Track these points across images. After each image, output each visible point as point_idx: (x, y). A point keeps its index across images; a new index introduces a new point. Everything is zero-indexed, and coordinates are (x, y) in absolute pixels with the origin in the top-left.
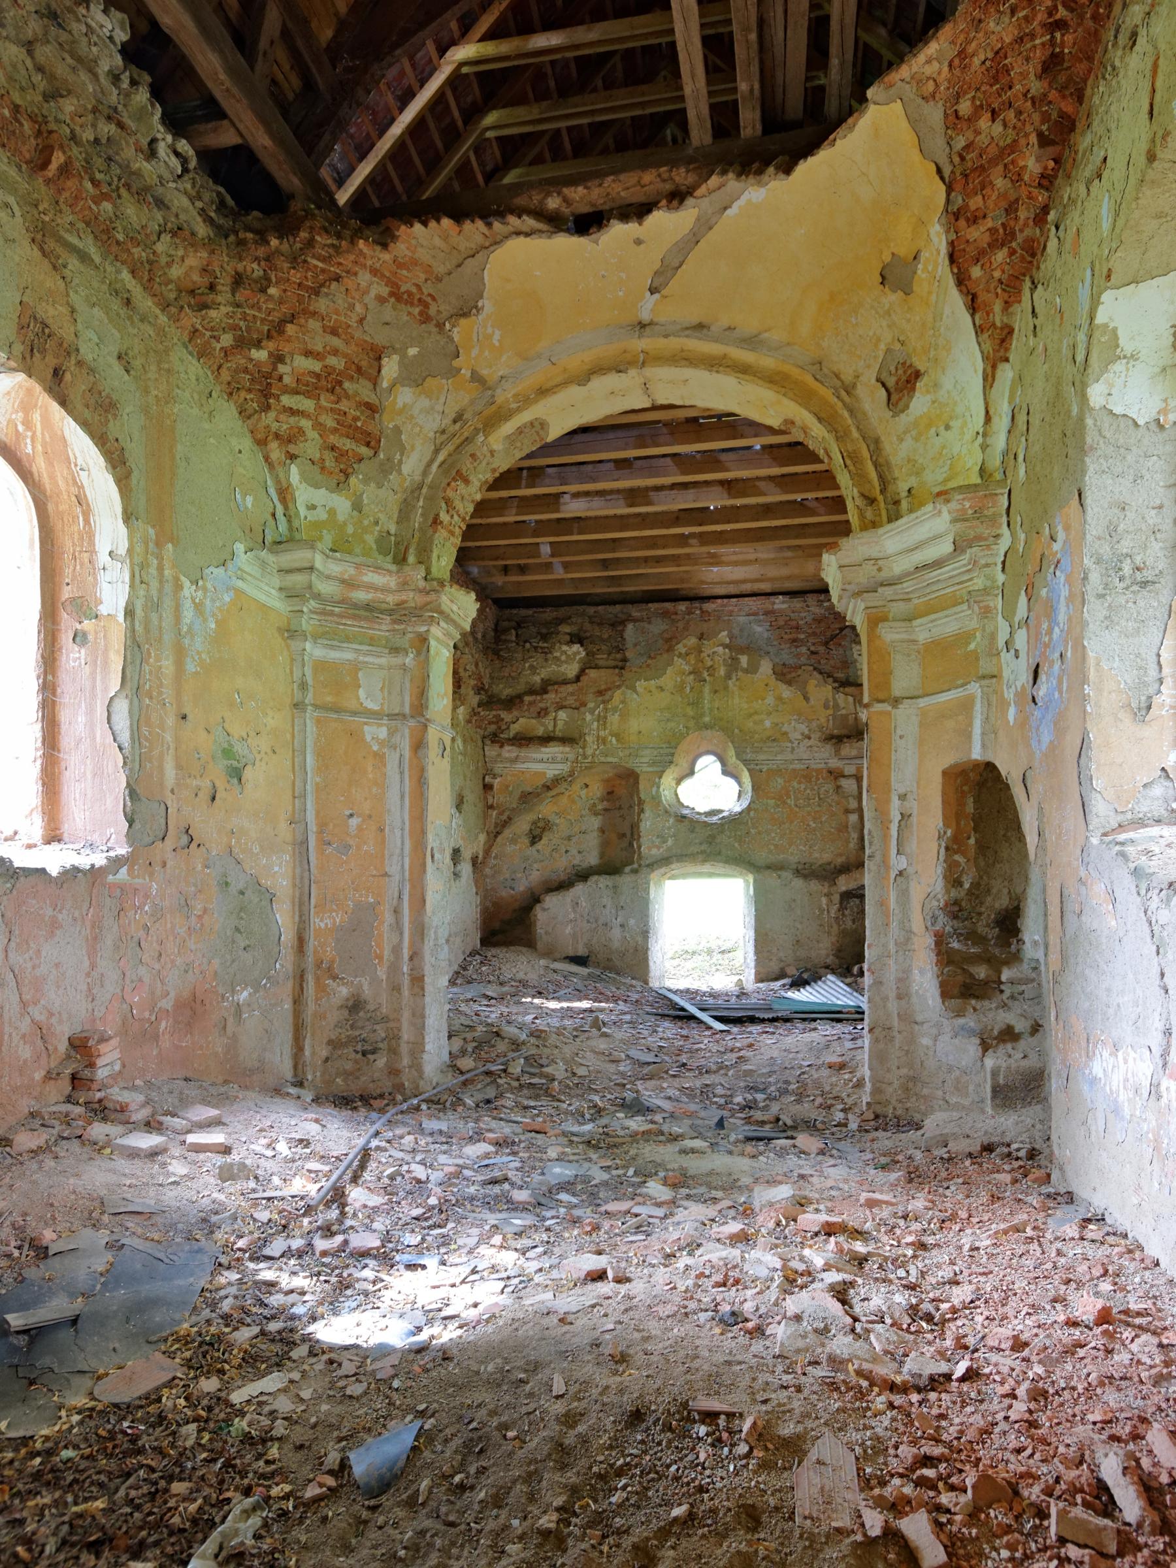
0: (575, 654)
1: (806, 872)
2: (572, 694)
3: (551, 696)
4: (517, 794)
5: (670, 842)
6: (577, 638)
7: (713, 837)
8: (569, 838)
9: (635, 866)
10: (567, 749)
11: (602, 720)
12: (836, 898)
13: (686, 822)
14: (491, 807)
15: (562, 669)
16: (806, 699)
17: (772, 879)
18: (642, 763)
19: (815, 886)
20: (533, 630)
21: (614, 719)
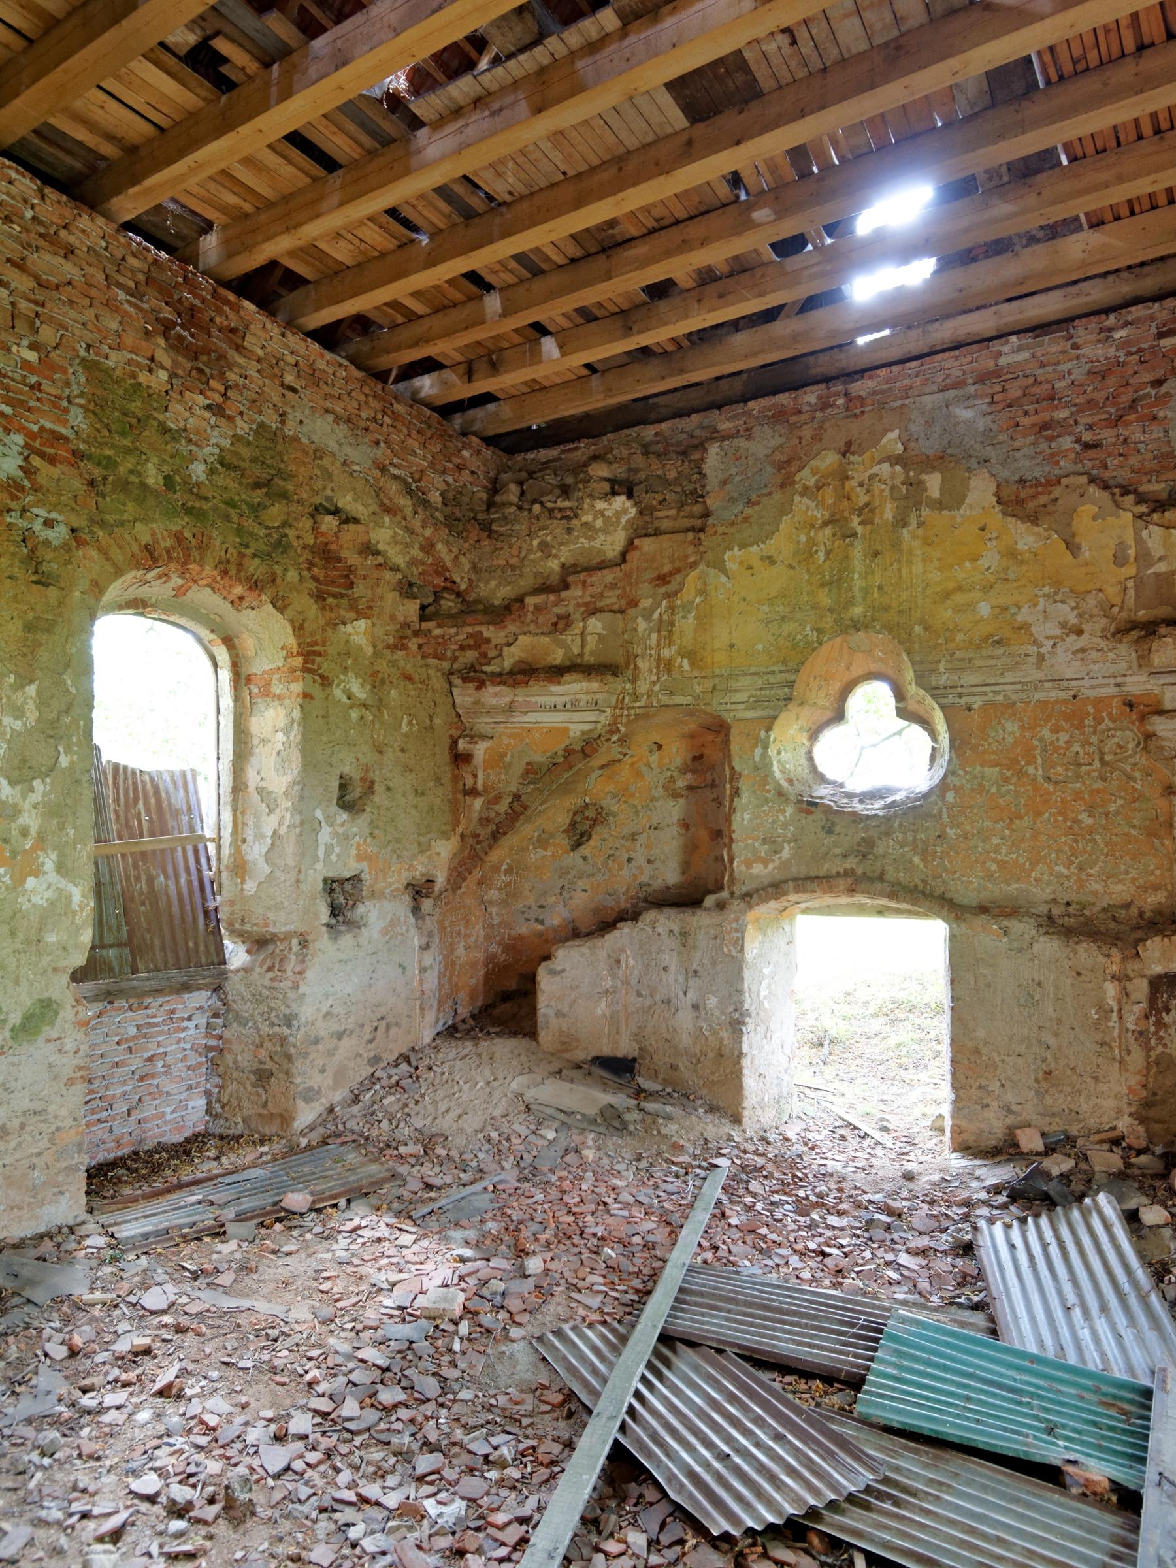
0: (618, 514)
1: (1072, 925)
2: (613, 586)
3: (575, 593)
4: (519, 768)
5: (786, 853)
6: (624, 487)
7: (869, 843)
8: (633, 837)
9: (725, 894)
10: (595, 685)
11: (665, 629)
12: (1141, 988)
13: (818, 815)
14: (473, 792)
15: (597, 543)
16: (1072, 546)
17: (987, 936)
18: (736, 707)
19: (1086, 953)
20: (552, 480)
21: (686, 625)
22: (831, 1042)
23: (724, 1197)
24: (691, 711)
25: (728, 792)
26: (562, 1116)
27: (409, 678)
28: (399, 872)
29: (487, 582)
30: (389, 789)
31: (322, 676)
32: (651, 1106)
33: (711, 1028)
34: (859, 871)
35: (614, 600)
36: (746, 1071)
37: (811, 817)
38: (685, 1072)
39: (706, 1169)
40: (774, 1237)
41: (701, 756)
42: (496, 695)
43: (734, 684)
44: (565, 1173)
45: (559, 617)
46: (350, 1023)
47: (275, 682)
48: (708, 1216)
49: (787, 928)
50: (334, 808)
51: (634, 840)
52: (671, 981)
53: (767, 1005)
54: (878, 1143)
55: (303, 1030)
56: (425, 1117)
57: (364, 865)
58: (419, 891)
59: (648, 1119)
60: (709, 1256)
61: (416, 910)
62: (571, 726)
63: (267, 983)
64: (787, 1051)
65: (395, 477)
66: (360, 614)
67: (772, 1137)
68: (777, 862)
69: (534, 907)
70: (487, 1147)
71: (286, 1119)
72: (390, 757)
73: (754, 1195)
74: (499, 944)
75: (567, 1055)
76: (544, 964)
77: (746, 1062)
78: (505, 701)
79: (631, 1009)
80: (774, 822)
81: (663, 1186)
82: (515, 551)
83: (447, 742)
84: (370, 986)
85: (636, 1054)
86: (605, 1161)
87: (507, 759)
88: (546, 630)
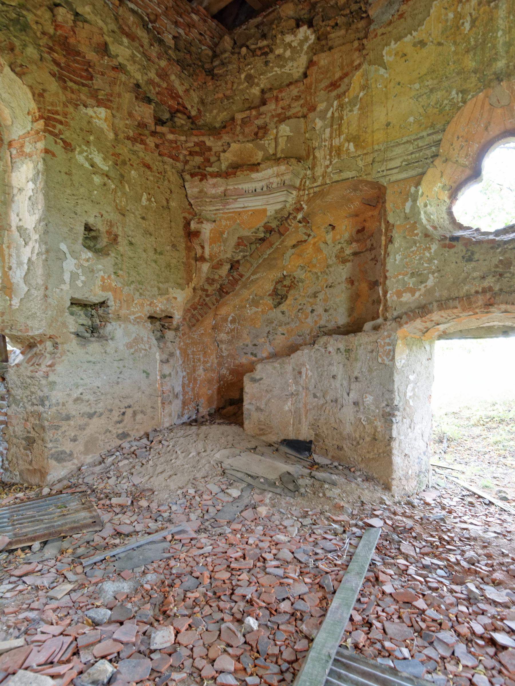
2: (298, 98)
4: (233, 241)
5: (431, 282)
9: (380, 321)
11: (336, 123)
13: (459, 247)
14: (202, 259)
15: (286, 70)
18: (391, 173)
21: (352, 116)
22: (448, 440)
23: (377, 558)
24: (356, 185)
25: (383, 243)
26: (249, 480)
27: (148, 167)
28: (142, 305)
29: (211, 112)
30: (131, 244)
31: (64, 142)
32: (320, 475)
33: (368, 419)
34: (497, 288)
35: (298, 109)
36: (395, 451)
37: (453, 250)
38: (348, 452)
39: (361, 528)
40: (431, 613)
41: (363, 229)
42: (214, 185)
43: (389, 155)
44: (239, 526)
45: (259, 128)
46: (100, 407)
47: (27, 144)
48: (363, 580)
49: (428, 348)
50: (79, 246)
51: (315, 297)
52: (338, 386)
53: (411, 403)
54: (502, 510)
55: (54, 409)
56: (144, 476)
57: (110, 295)
58: (160, 322)
59: (317, 484)
60: (361, 637)
61: (161, 338)
62: (268, 208)
63: (29, 374)
64: (426, 439)
65: (132, 11)
66: (100, 103)
67: (416, 502)
68: (423, 290)
69: (250, 345)
70: (183, 500)
71: (43, 473)
72: (130, 219)
73: (406, 557)
74: (228, 369)
75: (264, 438)
76: (248, 374)
77: (395, 445)
78: (220, 190)
79: (309, 407)
80: (421, 258)
81: (322, 543)
82: (229, 86)
83: (181, 224)
84: (118, 383)
85: (313, 439)
86: (277, 517)
87: (225, 236)
88: (250, 138)
